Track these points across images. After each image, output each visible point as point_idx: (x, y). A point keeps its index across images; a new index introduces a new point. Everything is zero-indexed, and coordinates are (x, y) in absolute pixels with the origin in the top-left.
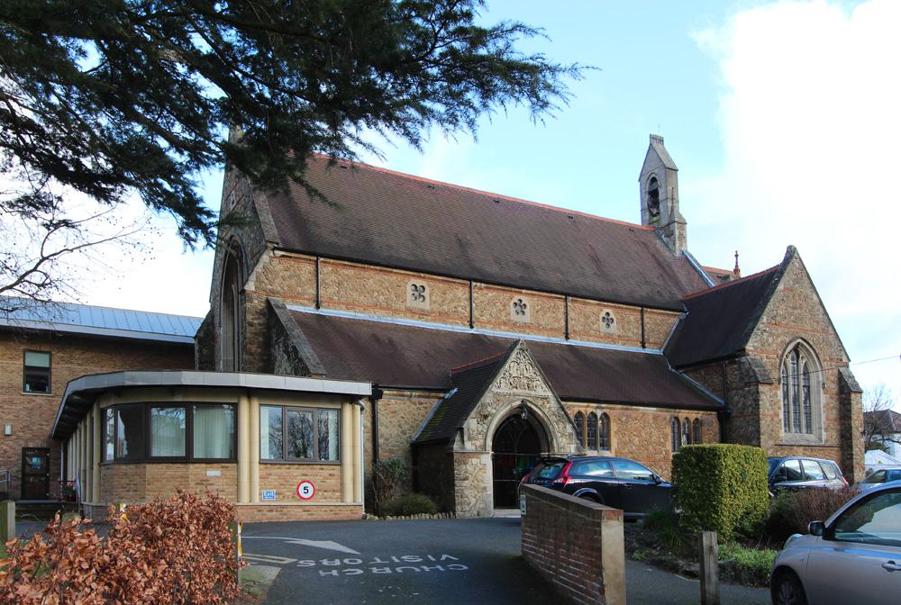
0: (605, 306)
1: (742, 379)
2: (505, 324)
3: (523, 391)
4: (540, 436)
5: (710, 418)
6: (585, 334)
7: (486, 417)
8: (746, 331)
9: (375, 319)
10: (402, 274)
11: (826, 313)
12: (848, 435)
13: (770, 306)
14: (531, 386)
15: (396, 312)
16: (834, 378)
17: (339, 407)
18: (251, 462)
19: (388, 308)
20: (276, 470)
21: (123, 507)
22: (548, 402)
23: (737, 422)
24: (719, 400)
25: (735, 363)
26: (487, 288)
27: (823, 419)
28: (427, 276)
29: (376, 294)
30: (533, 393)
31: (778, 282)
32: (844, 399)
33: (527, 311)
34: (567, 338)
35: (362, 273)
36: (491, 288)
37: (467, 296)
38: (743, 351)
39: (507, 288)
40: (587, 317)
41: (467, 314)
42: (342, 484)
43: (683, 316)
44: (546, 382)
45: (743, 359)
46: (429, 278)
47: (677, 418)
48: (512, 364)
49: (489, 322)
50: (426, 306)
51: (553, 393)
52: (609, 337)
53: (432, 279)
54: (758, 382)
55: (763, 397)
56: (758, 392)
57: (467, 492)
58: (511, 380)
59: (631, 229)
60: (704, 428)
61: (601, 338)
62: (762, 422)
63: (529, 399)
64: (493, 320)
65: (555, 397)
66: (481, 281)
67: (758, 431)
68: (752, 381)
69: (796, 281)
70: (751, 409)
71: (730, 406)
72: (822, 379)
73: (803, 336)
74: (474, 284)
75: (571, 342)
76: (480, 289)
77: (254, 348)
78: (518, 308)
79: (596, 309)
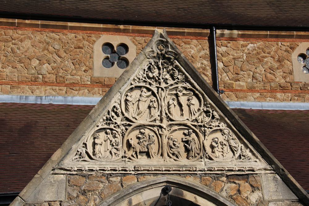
2: (283, 89)
3: (170, 162)
9: (32, 100)
10: (85, 29)
14: (194, 146)
15: (73, 86)
19: (59, 82)
22: (254, 188)
26: (243, 36)
28: (131, 27)
29: (35, 63)
30: (202, 165)
35: (11, 32)
36: (250, 36)
39: (283, 33)
46: (134, 31)
48: (136, 94)
51: (270, 161)
53: (139, 32)
58: (132, 137)
63: (190, 181)
64: (259, 86)
65: (277, 170)
66: (230, 27)
76: (231, 39)
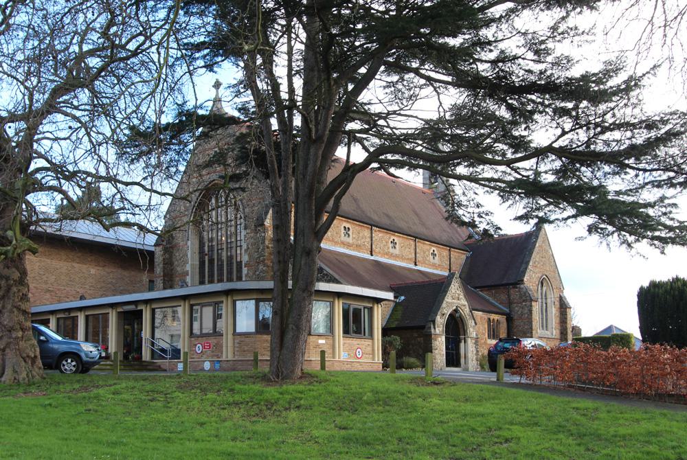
0: (433, 246)
1: (521, 297)
4: (460, 327)
5: (502, 319)
6: (424, 263)
7: (443, 315)
8: (521, 269)
11: (555, 261)
12: (565, 333)
13: (533, 256)
16: (558, 299)
17: (332, 300)
18: (227, 334)
20: (350, 341)
21: (570, 342)
23: (517, 323)
24: (505, 309)
25: (517, 288)
27: (554, 323)
31: (536, 242)
32: (563, 312)
33: (397, 246)
34: (416, 265)
37: (369, 235)
38: (522, 281)
40: (424, 253)
41: (370, 247)
42: (373, 350)
43: (469, 254)
44: (465, 296)
45: (522, 286)
47: (489, 319)
49: (380, 253)
50: (350, 240)
52: (434, 266)
54: (531, 300)
55: (534, 309)
56: (531, 306)
57: (437, 356)
59: (415, 189)
60: (501, 325)
61: (430, 265)
62: (533, 323)
67: (531, 328)
68: (528, 299)
69: (543, 242)
70: (526, 316)
71: (513, 313)
72: (552, 298)
73: (547, 274)
74: (417, 240)
75: (418, 268)
77: (269, 263)
78: (392, 245)
79: (428, 247)
